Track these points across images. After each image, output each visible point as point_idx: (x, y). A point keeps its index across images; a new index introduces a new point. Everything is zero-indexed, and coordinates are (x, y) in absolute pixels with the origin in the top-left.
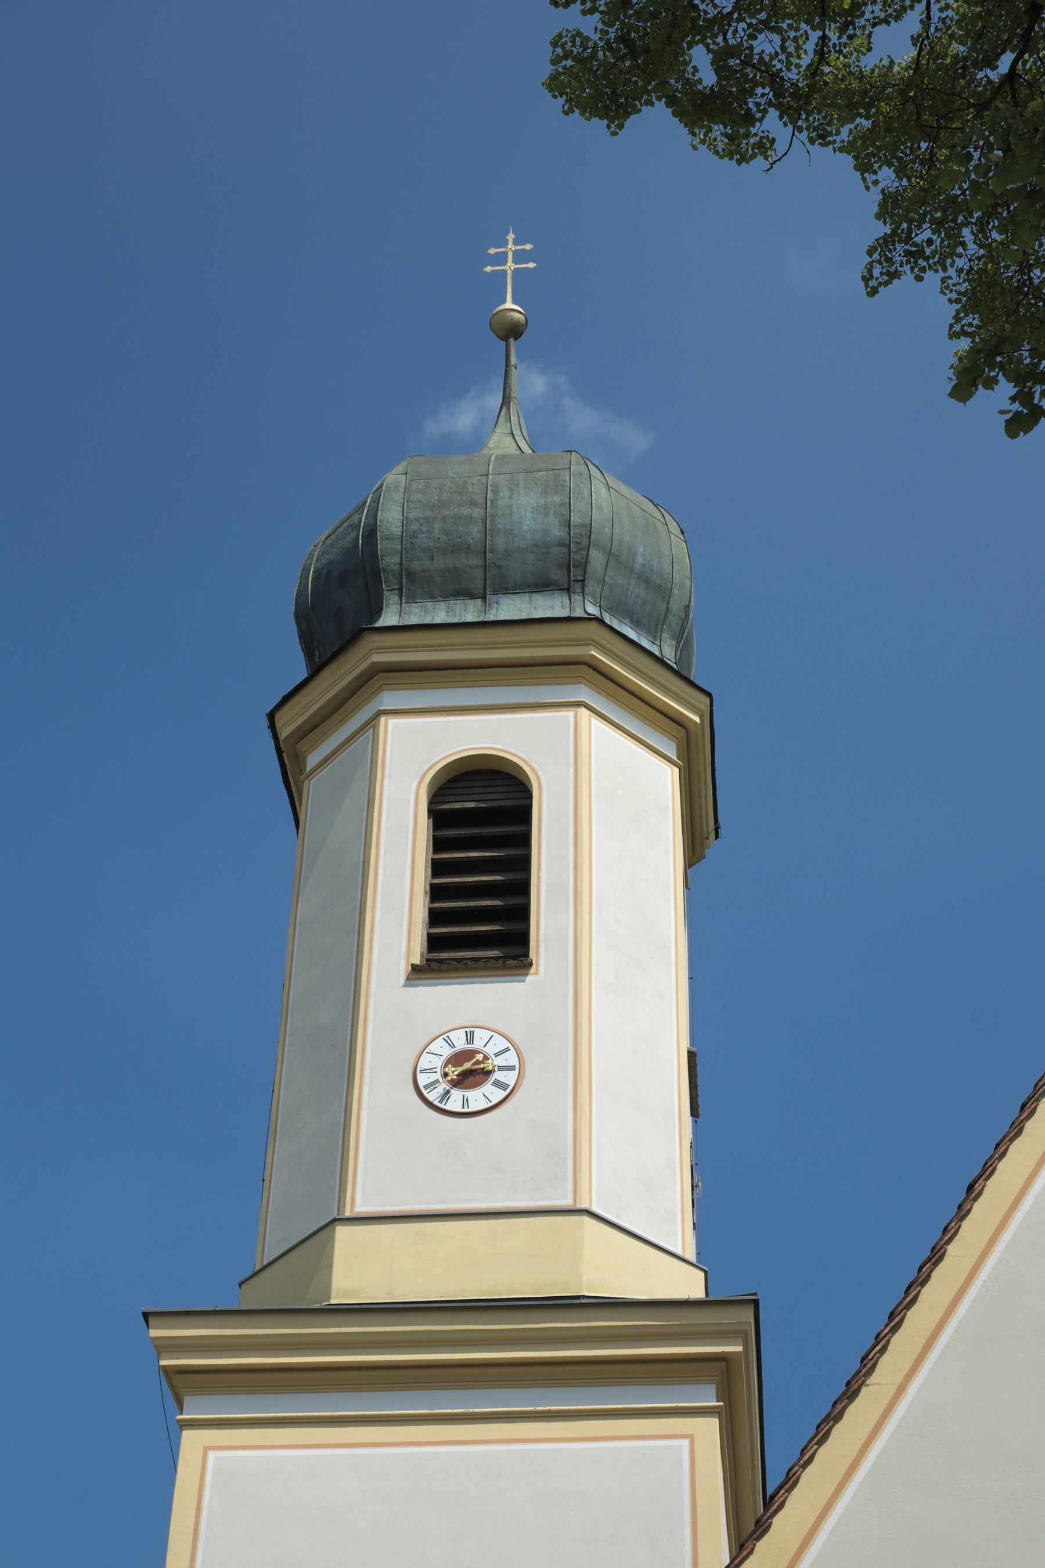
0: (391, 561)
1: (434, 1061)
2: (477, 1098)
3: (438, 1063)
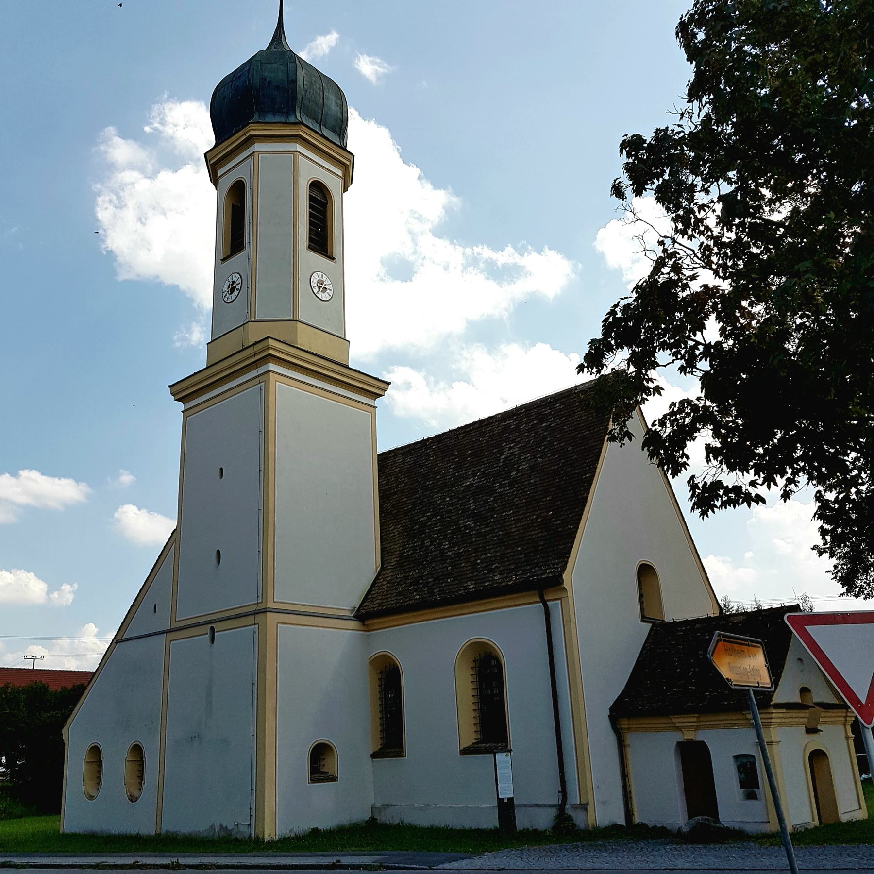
0: (299, 96)
1: (315, 279)
2: (325, 296)
3: (316, 281)
